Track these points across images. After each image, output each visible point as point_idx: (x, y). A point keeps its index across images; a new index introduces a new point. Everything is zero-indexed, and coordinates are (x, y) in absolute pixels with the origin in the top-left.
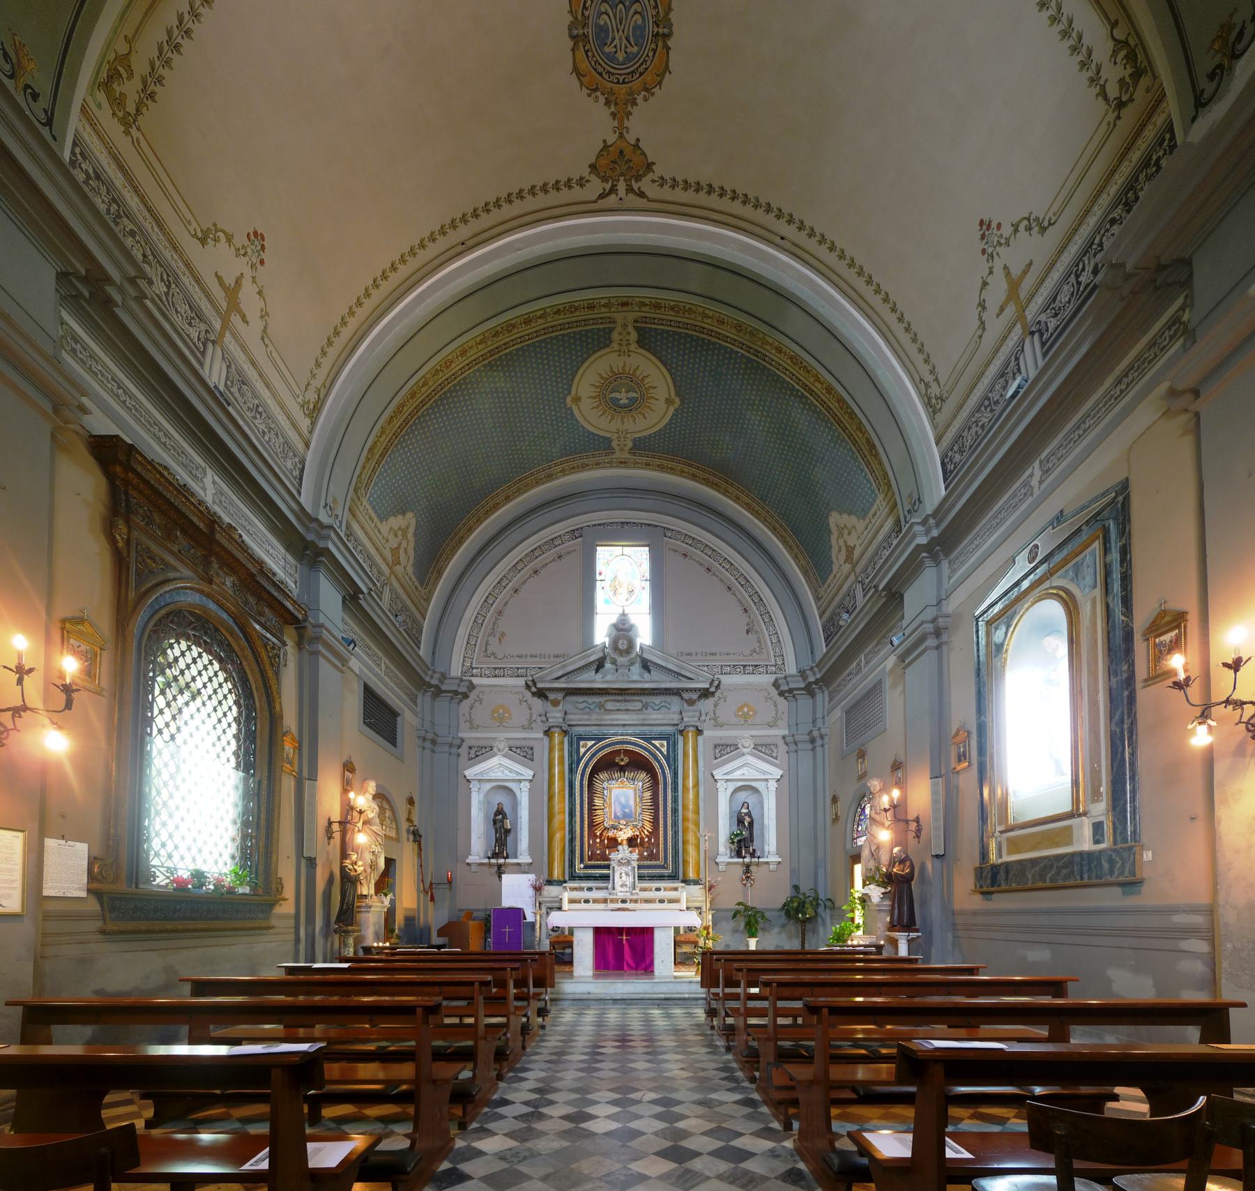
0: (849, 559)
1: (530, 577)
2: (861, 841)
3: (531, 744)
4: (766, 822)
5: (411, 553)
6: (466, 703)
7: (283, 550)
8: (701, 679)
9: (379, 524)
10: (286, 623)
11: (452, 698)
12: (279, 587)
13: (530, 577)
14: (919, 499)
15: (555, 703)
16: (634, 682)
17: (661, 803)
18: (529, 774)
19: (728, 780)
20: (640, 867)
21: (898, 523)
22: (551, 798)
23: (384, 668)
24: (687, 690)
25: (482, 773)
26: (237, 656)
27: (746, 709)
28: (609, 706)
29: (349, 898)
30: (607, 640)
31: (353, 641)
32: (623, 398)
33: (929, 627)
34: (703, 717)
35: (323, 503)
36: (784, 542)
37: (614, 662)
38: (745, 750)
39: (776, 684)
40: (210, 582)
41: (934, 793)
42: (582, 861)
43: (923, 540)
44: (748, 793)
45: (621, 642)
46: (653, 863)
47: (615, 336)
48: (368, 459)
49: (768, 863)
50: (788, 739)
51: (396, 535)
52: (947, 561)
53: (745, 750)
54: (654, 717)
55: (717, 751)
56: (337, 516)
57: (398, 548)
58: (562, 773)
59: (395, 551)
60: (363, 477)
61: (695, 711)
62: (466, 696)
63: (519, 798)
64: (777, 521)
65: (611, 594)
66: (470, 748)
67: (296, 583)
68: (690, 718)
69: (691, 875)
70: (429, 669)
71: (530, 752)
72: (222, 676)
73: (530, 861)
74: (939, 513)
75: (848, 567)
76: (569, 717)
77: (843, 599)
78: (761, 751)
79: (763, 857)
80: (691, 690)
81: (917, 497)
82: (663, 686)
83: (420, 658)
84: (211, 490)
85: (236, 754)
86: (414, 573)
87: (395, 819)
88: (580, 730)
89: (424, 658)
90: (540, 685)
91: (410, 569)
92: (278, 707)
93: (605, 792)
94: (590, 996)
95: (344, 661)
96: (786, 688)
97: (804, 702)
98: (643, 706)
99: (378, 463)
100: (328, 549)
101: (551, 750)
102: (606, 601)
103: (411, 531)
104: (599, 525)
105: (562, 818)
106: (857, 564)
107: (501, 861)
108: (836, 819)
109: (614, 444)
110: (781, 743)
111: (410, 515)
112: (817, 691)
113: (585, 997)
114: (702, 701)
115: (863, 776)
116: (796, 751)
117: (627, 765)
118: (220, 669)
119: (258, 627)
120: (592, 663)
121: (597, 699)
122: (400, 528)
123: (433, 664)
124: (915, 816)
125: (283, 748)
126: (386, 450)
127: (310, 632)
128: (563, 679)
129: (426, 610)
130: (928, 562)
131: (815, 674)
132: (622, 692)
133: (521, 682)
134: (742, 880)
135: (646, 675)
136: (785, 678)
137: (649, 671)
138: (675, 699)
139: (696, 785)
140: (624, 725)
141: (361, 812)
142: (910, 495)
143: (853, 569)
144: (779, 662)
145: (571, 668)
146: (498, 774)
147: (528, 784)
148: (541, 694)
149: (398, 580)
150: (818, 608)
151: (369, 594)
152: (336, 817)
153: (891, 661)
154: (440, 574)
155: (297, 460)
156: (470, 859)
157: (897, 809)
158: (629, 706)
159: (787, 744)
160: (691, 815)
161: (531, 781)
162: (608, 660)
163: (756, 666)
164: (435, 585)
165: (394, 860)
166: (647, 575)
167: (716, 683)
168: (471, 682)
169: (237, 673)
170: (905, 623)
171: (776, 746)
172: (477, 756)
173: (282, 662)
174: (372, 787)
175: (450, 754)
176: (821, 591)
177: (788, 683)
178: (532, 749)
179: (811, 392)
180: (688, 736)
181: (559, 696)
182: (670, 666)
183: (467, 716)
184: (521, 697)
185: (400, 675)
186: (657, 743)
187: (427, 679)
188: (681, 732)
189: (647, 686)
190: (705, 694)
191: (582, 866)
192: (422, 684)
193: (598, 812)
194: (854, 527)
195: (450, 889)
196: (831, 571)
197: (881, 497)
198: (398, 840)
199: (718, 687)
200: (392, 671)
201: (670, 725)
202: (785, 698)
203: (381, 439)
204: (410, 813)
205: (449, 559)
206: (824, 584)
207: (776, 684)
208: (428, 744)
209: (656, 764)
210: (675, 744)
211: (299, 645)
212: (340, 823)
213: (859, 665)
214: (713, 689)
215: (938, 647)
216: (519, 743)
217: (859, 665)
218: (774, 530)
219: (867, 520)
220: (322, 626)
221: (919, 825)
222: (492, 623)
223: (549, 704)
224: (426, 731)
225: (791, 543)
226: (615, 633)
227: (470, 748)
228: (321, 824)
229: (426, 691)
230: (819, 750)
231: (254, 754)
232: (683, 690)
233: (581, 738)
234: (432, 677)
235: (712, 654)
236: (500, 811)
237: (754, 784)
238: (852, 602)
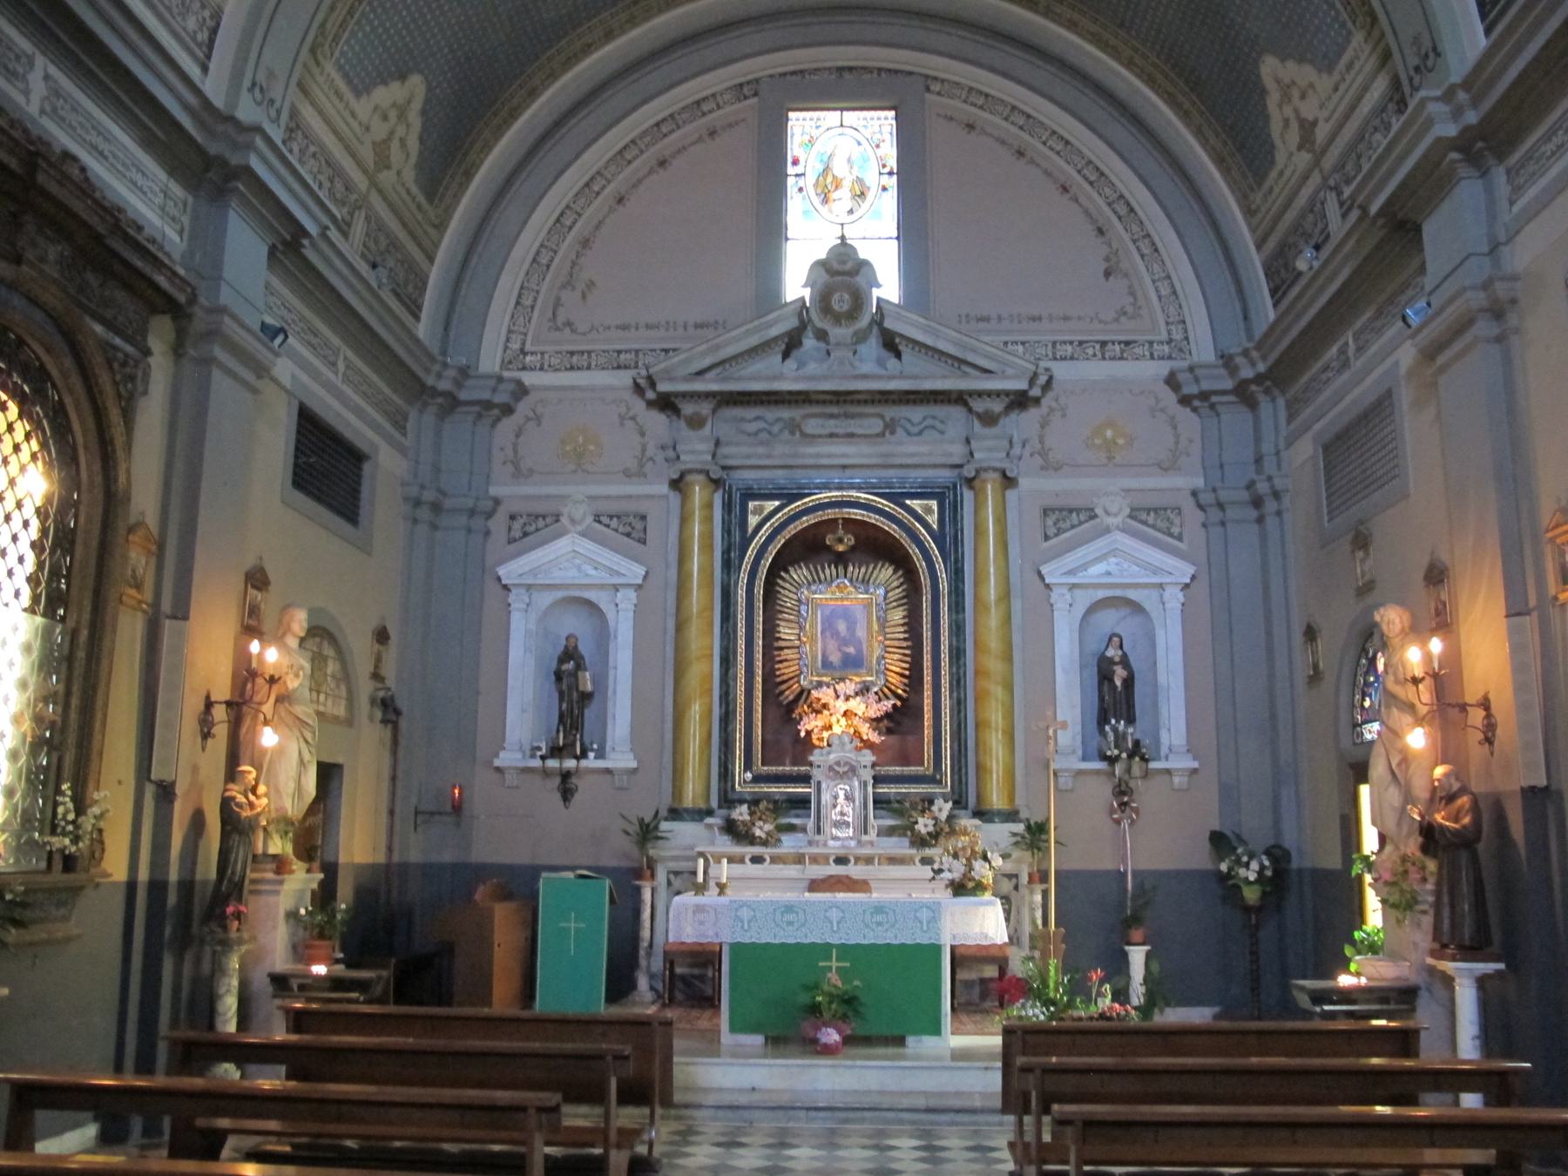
0: (1306, 141)
2: (1371, 731)
3: (642, 507)
4: (1162, 678)
5: (413, 145)
6: (507, 425)
7: (162, 175)
8: (1010, 371)
10: (154, 310)
11: (479, 416)
12: (148, 252)
13: (651, 172)
14: (1435, 49)
15: (696, 423)
16: (865, 377)
17: (927, 634)
18: (636, 572)
19: (1073, 587)
20: (877, 780)
21: (1396, 84)
23: (341, 366)
24: (980, 394)
25: (534, 572)
26: (54, 386)
28: (812, 426)
29: (239, 856)
30: (807, 293)
31: (282, 330)
33: (1478, 299)
34: (1017, 451)
35: (247, 83)
37: (822, 335)
38: (1111, 521)
39: (1172, 381)
40: (18, 260)
41: (1517, 649)
42: (748, 765)
43: (1451, 130)
44: (1124, 611)
45: (836, 296)
49: (1168, 772)
50: (1207, 498)
51: (385, 118)
52: (1501, 170)
53: (1111, 521)
54: (912, 449)
55: (1050, 522)
58: (707, 571)
59: (381, 149)
60: (329, 26)
61: (996, 437)
62: (508, 410)
63: (611, 624)
64: (1154, 65)
65: (816, 201)
66: (512, 517)
67: (181, 233)
69: (996, 800)
70: (432, 359)
71: (639, 525)
72: (21, 428)
73: (634, 764)
74: (1474, 83)
75: (1304, 158)
76: (724, 450)
77: (1302, 216)
78: (1145, 523)
79: (1158, 758)
80: (989, 394)
81: (1430, 45)
82: (928, 385)
83: (417, 341)
84: (38, 87)
85: (32, 580)
86: (416, 181)
87: (346, 676)
88: (749, 476)
89: (427, 343)
90: (663, 387)
91: (409, 175)
92: (122, 479)
93: (803, 608)
94: (755, 1098)
95: (261, 370)
96: (1193, 390)
97: (1235, 418)
98: (886, 426)
100: (248, 171)
101: (684, 520)
103: (417, 105)
104: (794, 73)
105: (704, 668)
106: (1324, 152)
107: (570, 764)
108: (1315, 677)
110: (1188, 505)
111: (416, 82)
112: (1261, 398)
113: (743, 1100)
114: (1013, 416)
115: (1366, 589)
116: (1223, 524)
117: (853, 549)
118: (20, 417)
119: (98, 329)
120: (775, 339)
121: (786, 413)
122: (394, 105)
123: (444, 353)
124: (1480, 695)
125: (125, 558)
127: (200, 321)
129: (436, 246)
130: (1463, 170)
131: (1253, 364)
132: (840, 398)
133: (624, 378)
134: (1112, 811)
135: (892, 363)
136: (1191, 369)
137: (898, 355)
138: (957, 412)
139: (1006, 596)
140: (844, 467)
141: (272, 680)
142: (1416, 40)
143: (1317, 162)
144: (1178, 335)
146: (568, 575)
147: (632, 594)
148: (666, 404)
149: (385, 199)
150: (1253, 230)
151: (323, 235)
152: (222, 690)
153: (1406, 355)
154: (468, 176)
155: (207, 13)
157: (1444, 680)
158: (854, 426)
159: (1201, 507)
160: (994, 665)
161: (639, 587)
163: (1127, 343)
166: (892, 163)
167: (1042, 379)
168: (519, 383)
169: (49, 423)
170: (1429, 281)
171: (1178, 510)
172: (526, 534)
173: (140, 389)
175: (469, 531)
176: (1258, 198)
177: (1197, 380)
180: (984, 490)
181: (705, 408)
183: (509, 452)
184: (623, 410)
185: (374, 377)
186: (915, 504)
187: (430, 381)
188: (970, 482)
190: (1020, 401)
191: (749, 775)
192: (418, 391)
194: (1311, 86)
195: (458, 825)
196: (1273, 163)
197: (1358, 38)
198: (349, 722)
200: (359, 372)
201: (944, 466)
202: (1195, 410)
204: (378, 660)
205: (487, 147)
206: (1260, 185)
207: (1172, 381)
208: (424, 513)
209: (914, 551)
210: (956, 507)
211: (177, 351)
212: (229, 704)
213: (1343, 351)
214: (1035, 392)
215: (1500, 339)
216: (614, 507)
217: (1343, 351)
219: (1336, 76)
220: (223, 310)
221: (1489, 716)
222: (569, 264)
223: (682, 424)
225: (1187, 105)
226: (824, 277)
227: (512, 517)
228: (192, 706)
229: (425, 405)
230: (1271, 521)
231: (68, 577)
232: (971, 393)
234: (439, 376)
235: (1034, 319)
236: (570, 654)
237: (1132, 595)
238: (1320, 226)
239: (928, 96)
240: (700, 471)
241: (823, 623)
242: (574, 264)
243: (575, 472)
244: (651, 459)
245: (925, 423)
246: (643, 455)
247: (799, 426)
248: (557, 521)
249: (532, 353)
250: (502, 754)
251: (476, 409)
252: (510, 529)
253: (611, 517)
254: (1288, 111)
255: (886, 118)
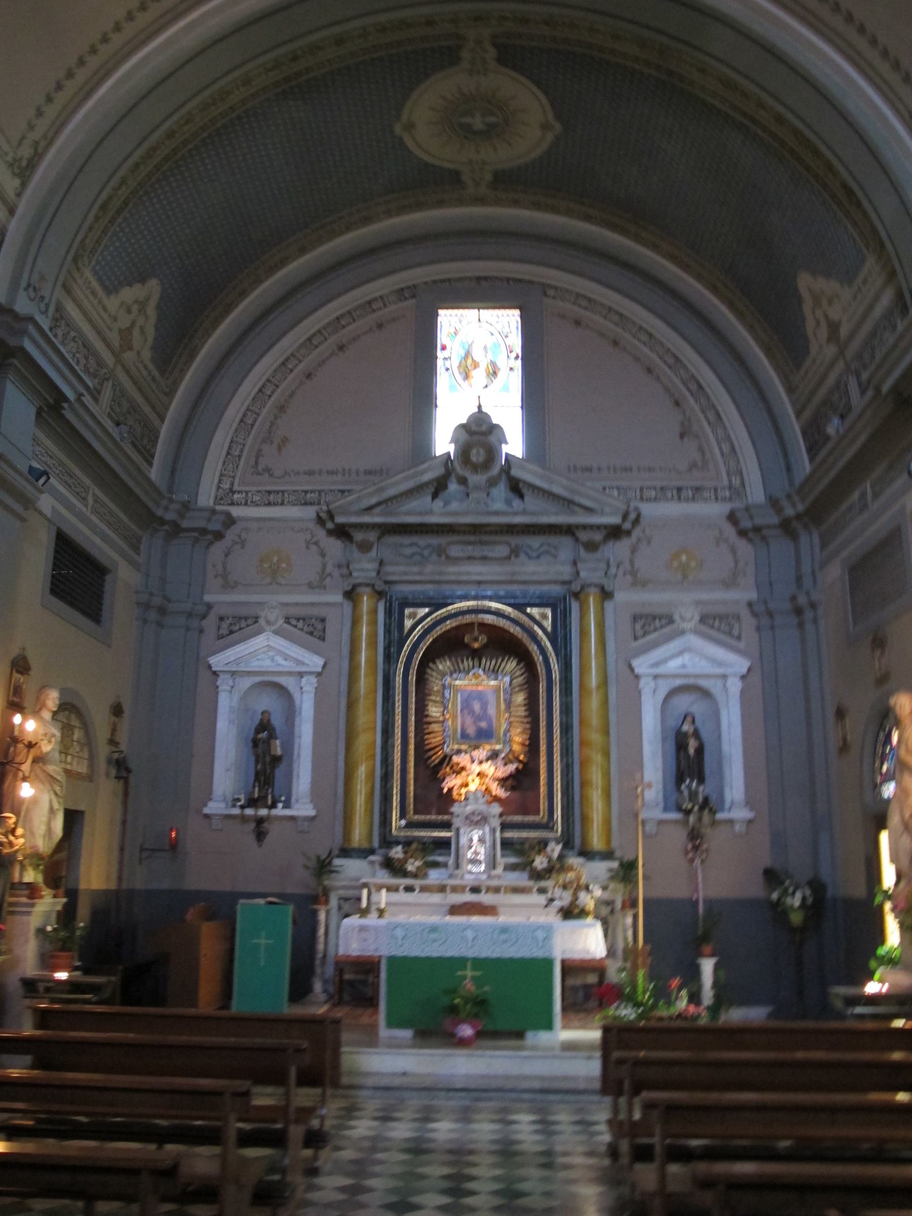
1: (333, 354)
3: (321, 612)
4: (726, 748)
5: (151, 332)
6: (218, 549)
9: (106, 301)
11: (197, 540)
15: (365, 547)
16: (497, 513)
18: (316, 662)
20: (504, 827)
22: (351, 705)
24: (585, 527)
25: (237, 661)
27: (684, 558)
28: (455, 551)
30: (451, 449)
31: (45, 473)
32: (478, 123)
34: (613, 570)
35: (23, 284)
36: (731, 305)
37: (463, 481)
38: (687, 626)
39: (732, 518)
42: (403, 815)
45: (474, 452)
46: (530, 818)
47: (465, 54)
48: (97, 218)
51: (129, 311)
53: (687, 626)
55: (638, 626)
56: (42, 298)
57: (129, 330)
58: (372, 662)
62: (219, 536)
63: (297, 702)
66: (221, 619)
68: (590, 572)
69: (597, 842)
71: (320, 626)
73: (312, 813)
75: (831, 351)
76: (388, 568)
82: (544, 520)
87: (89, 742)
88: (406, 589)
90: (340, 519)
91: (147, 354)
94: (405, 1081)
95: (28, 503)
97: (781, 546)
98: (512, 551)
99: (112, 221)
100: (23, 350)
101: (355, 622)
102: (452, 388)
103: (153, 303)
107: (263, 812)
108: (844, 748)
109: (465, 178)
110: (745, 613)
113: (397, 1082)
114: (610, 544)
116: (772, 628)
117: (485, 647)
121: (434, 541)
123: (170, 491)
126: (126, 203)
128: (378, 510)
129: (167, 408)
131: (794, 505)
132: (476, 529)
134: (686, 852)
135: (517, 503)
136: (747, 509)
137: (521, 496)
138: (566, 542)
139: (604, 683)
141: (30, 745)
143: (841, 352)
144: (736, 482)
145: (392, 492)
146: (264, 663)
147: (314, 680)
148: (342, 532)
150: (793, 403)
154: (192, 356)
156: (215, 807)
158: (487, 551)
160: (595, 737)
161: (319, 674)
162: (453, 479)
164: (183, 372)
165: (81, 813)
166: (518, 350)
167: (633, 516)
168: (228, 515)
171: (738, 618)
172: (231, 632)
174: (52, 698)
178: (323, 620)
179: (753, 120)
181: (372, 536)
182: (556, 489)
183: (220, 568)
184: (308, 536)
185: (112, 506)
186: (534, 611)
187: (159, 512)
188: (576, 595)
189: (518, 520)
190: (615, 533)
191: (403, 822)
193: (435, 727)
199: (637, 521)
203: (120, 192)
205: (208, 334)
207: (732, 518)
208: (153, 615)
209: (533, 648)
213: (863, 495)
216: (302, 612)
218: (714, 289)
223: (354, 548)
224: (151, 594)
226: (464, 436)
227: (221, 619)
230: (809, 627)
233: (406, 603)
234: (166, 509)
236: (265, 726)
237: (704, 683)
239: (545, 300)
240: (367, 585)
241: (462, 704)
242: (272, 424)
243: (271, 584)
244: (330, 575)
245: (542, 549)
246: (323, 573)
247: (445, 550)
248: (256, 622)
249: (239, 492)
250: (211, 804)
251: (196, 534)
252: (219, 628)
253: (298, 620)
254: (819, 313)
255: (514, 315)
